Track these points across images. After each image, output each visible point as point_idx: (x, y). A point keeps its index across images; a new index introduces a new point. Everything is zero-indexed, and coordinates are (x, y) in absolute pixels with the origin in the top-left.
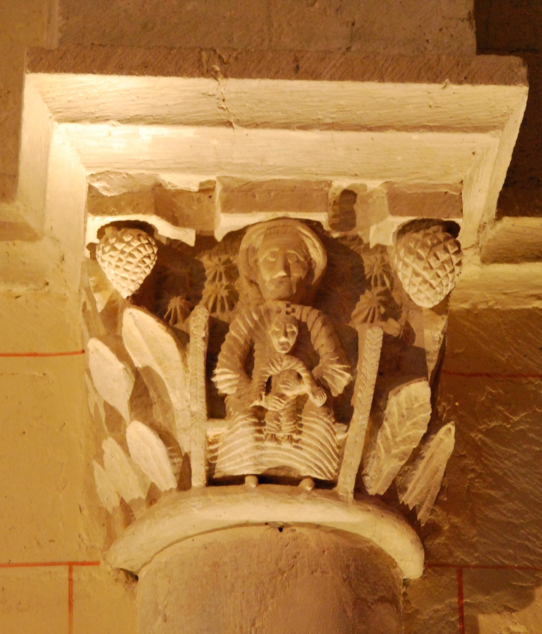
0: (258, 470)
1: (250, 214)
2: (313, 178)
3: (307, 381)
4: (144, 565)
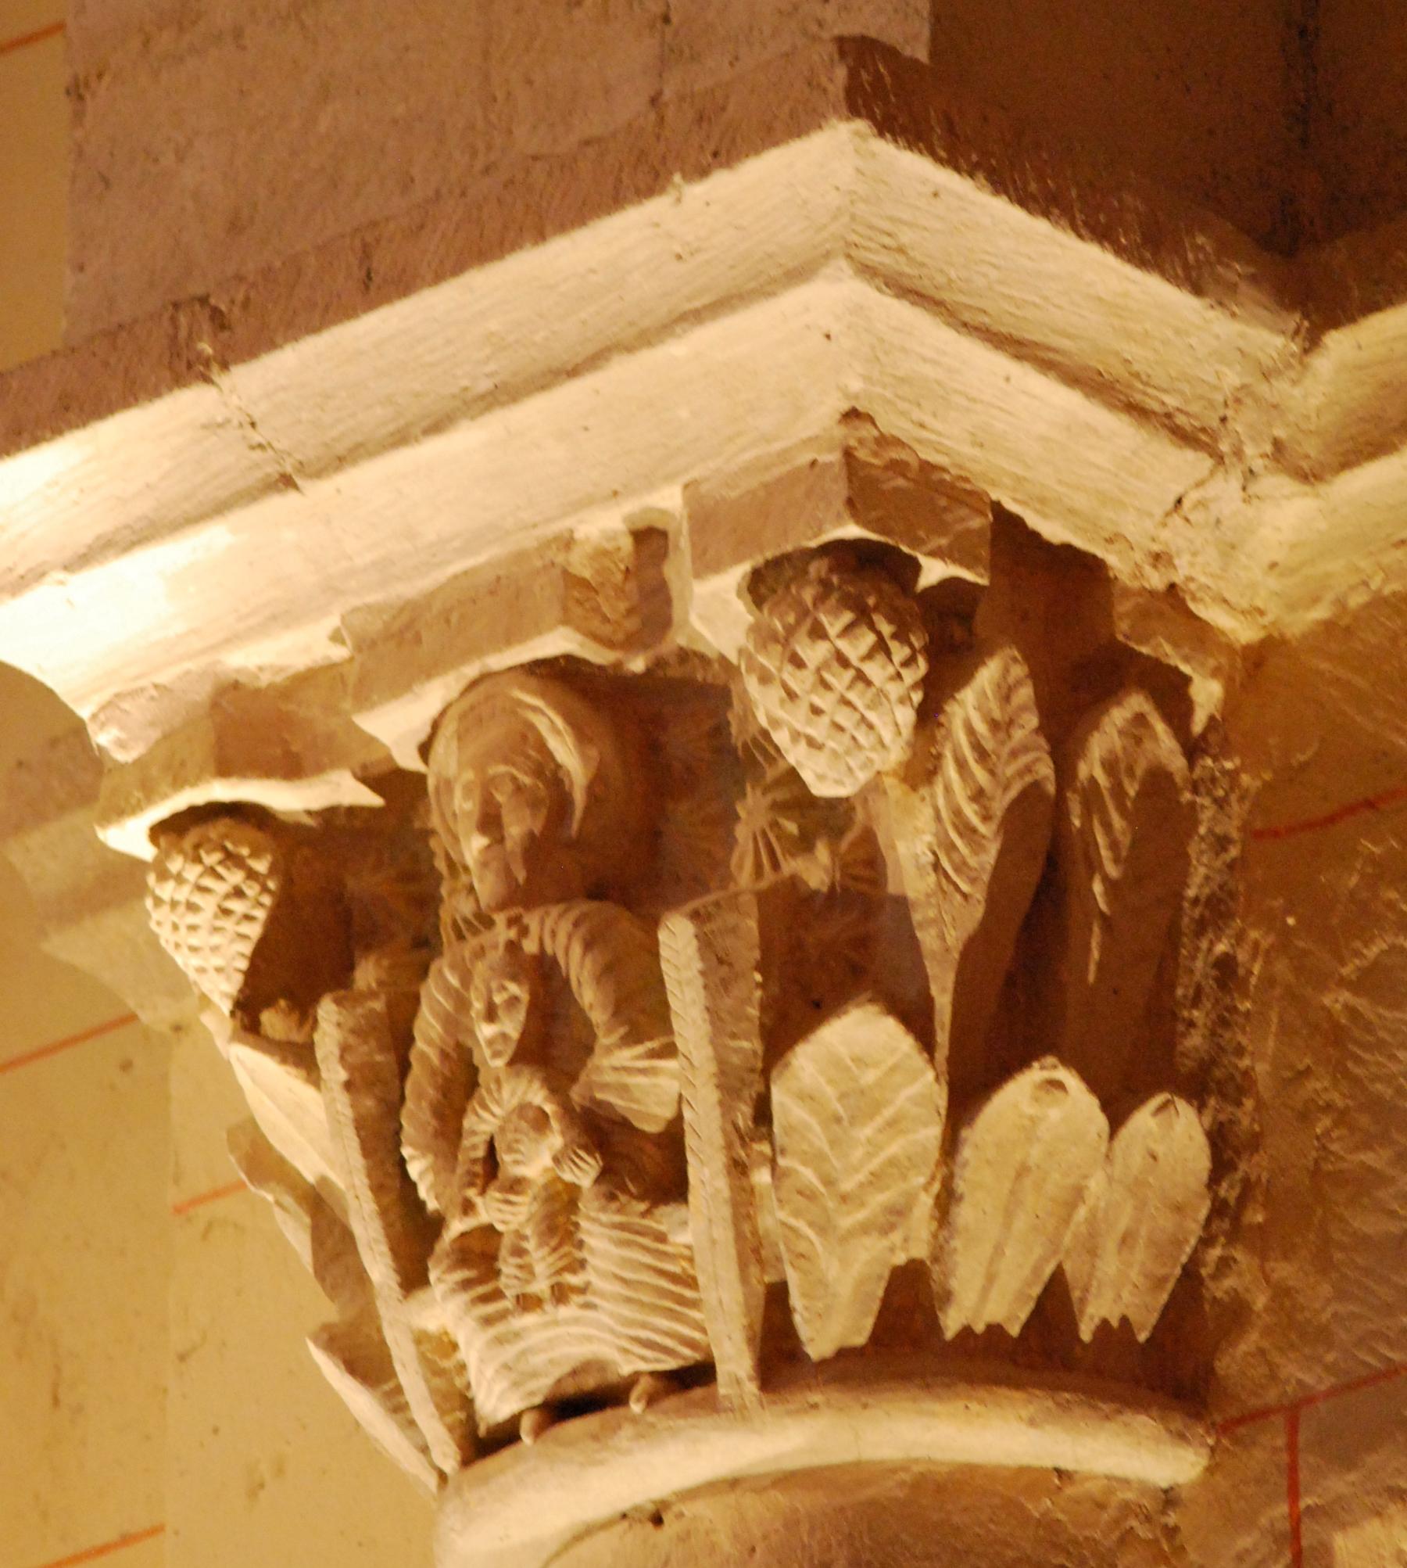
0: (532, 1394)
1: (409, 696)
2: (528, 541)
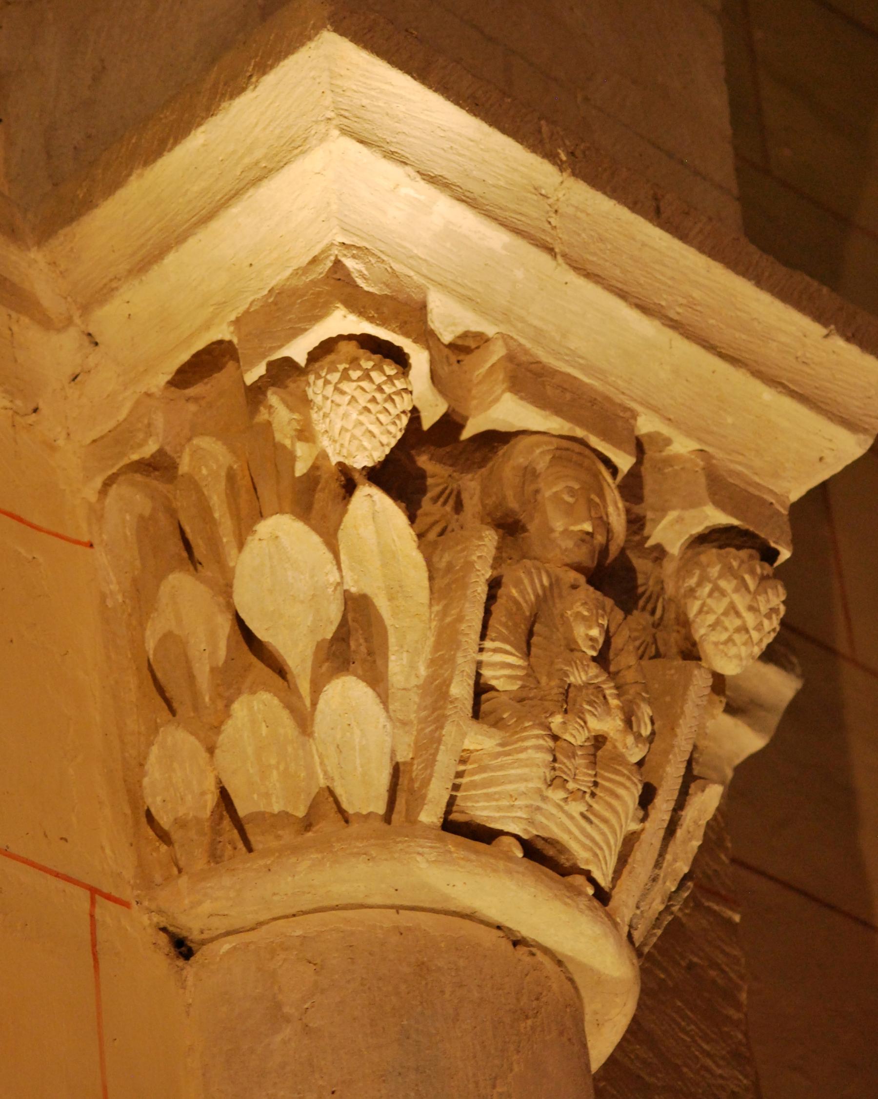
3: (620, 716)
4: (228, 933)
